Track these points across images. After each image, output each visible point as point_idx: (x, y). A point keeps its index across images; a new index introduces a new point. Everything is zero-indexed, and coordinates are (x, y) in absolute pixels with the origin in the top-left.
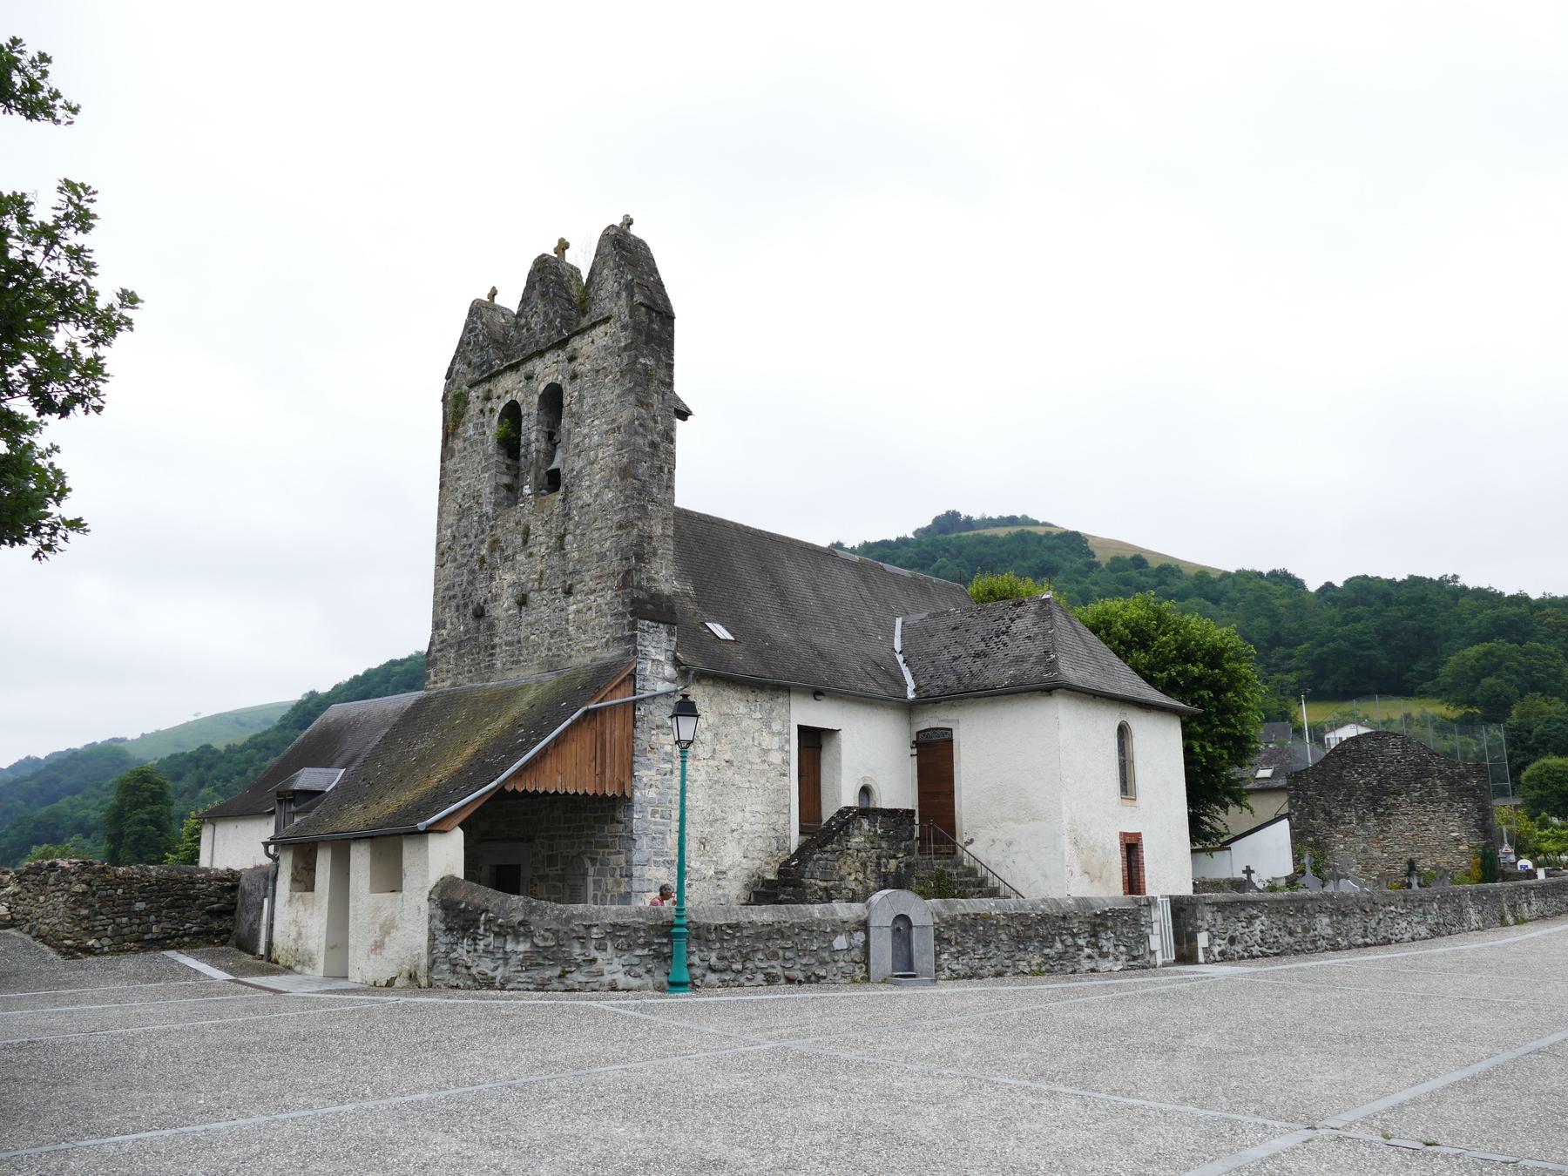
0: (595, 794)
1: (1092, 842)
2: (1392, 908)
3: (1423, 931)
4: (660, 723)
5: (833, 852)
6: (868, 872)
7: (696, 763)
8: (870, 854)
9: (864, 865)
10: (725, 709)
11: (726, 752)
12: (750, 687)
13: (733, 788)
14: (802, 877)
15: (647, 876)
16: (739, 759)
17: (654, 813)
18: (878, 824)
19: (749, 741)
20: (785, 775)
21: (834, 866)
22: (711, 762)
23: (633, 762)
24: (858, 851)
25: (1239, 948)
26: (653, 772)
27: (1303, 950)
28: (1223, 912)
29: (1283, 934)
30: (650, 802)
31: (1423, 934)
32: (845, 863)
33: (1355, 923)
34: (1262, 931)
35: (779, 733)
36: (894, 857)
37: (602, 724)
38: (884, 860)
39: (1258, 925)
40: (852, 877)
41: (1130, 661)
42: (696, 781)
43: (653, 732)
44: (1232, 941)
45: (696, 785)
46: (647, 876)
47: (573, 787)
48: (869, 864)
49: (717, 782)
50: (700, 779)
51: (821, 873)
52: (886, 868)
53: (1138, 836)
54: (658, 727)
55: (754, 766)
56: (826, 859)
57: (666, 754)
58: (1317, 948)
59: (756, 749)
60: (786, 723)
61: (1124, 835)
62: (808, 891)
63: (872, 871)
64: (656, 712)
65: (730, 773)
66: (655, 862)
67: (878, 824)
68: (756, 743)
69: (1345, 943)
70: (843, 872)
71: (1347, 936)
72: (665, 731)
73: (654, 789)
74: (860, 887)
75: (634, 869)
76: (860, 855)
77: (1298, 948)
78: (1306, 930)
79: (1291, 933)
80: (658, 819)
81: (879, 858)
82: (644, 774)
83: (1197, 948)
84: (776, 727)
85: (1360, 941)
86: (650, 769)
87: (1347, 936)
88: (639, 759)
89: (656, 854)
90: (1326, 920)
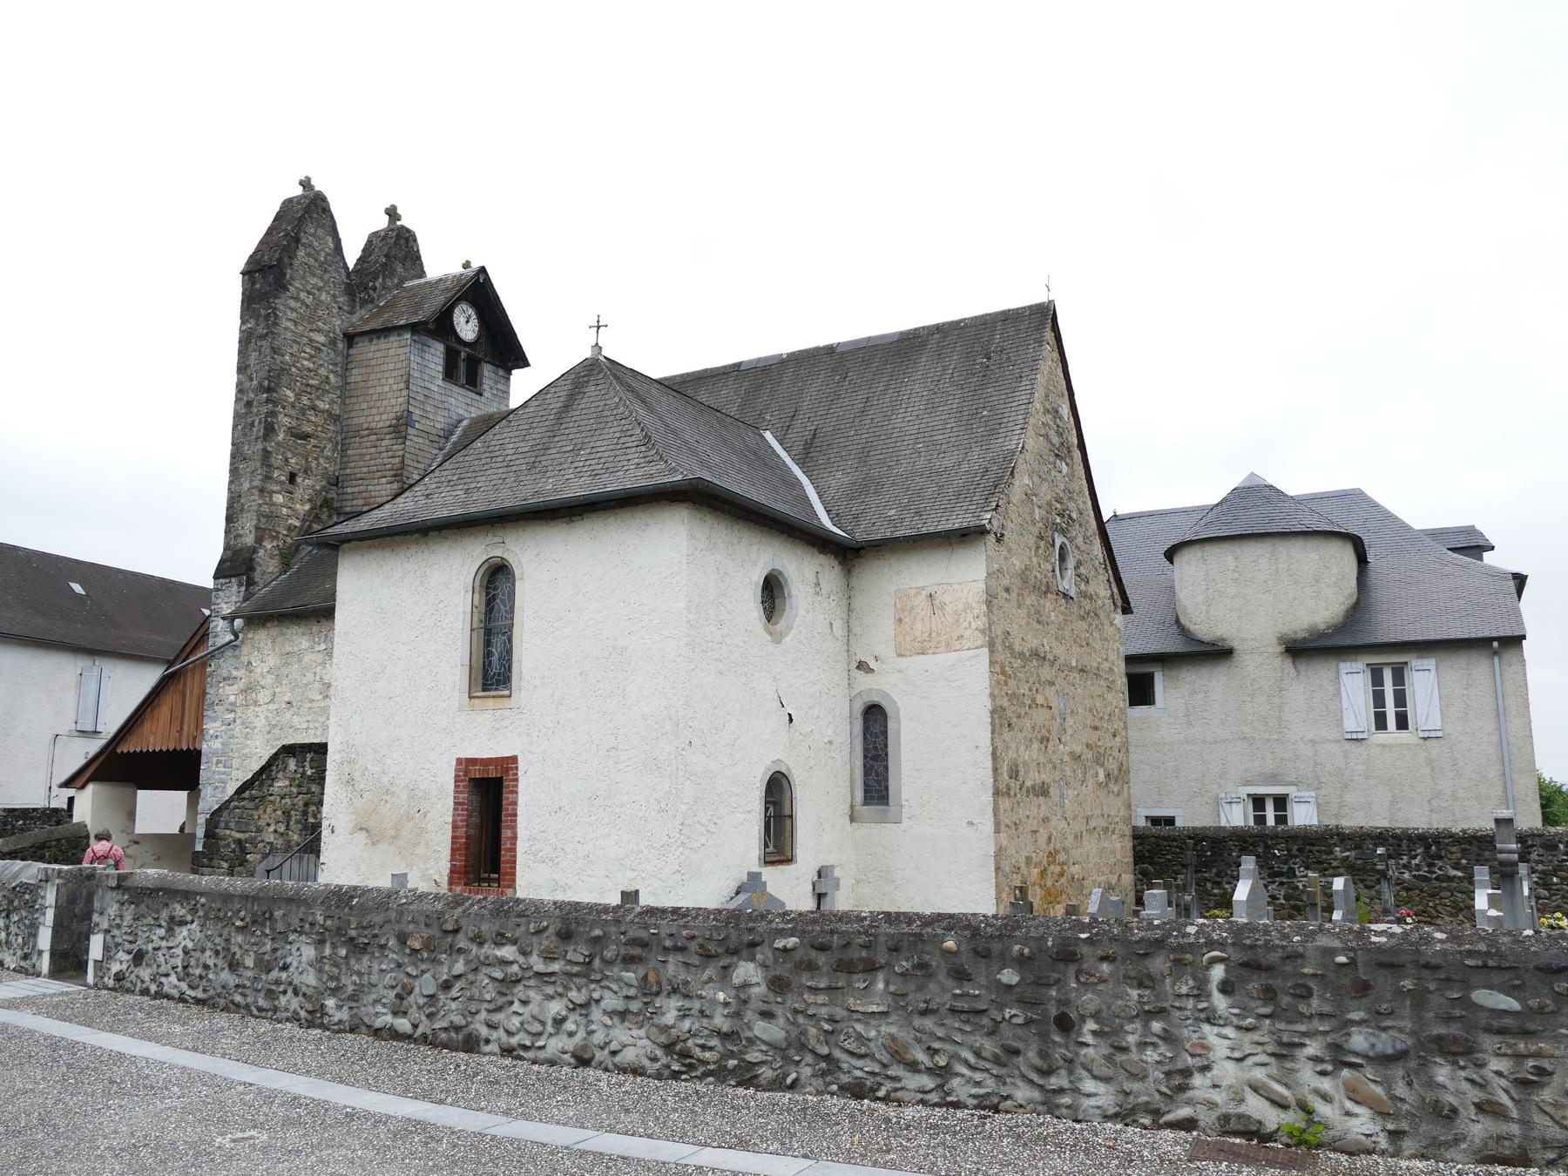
0: (175, 749)
1: (385, 780)
2: (508, 952)
3: (636, 1044)
5: (252, 799)
6: (292, 823)
7: (256, 709)
9: (287, 814)
10: (288, 648)
12: (314, 617)
13: (292, 730)
16: (299, 699)
17: (218, 762)
18: (307, 764)
19: (310, 676)
22: (271, 706)
23: (203, 716)
25: (145, 973)
26: (218, 724)
27: (247, 1007)
28: (137, 905)
29: (220, 963)
30: (215, 753)
31: (629, 1055)
33: (380, 971)
34: (186, 952)
37: (185, 685)
39: (185, 937)
40: (271, 829)
41: (233, 486)
42: (255, 727)
44: (138, 958)
45: (256, 731)
49: (275, 725)
51: (237, 822)
53: (508, 764)
54: (224, 679)
57: (231, 704)
58: (275, 1009)
59: (317, 685)
61: (465, 764)
62: (222, 843)
63: (297, 822)
64: (223, 665)
65: (288, 715)
67: (307, 764)
68: (318, 678)
69: (344, 1015)
70: (262, 823)
71: (354, 997)
72: (231, 682)
73: (220, 740)
74: (280, 841)
75: (451, 820)
76: (283, 801)
77: (238, 998)
78: (264, 966)
79: (234, 966)
81: (306, 805)
82: (211, 727)
83: (87, 962)
85: (387, 1019)
87: (354, 997)
90: (309, 952)
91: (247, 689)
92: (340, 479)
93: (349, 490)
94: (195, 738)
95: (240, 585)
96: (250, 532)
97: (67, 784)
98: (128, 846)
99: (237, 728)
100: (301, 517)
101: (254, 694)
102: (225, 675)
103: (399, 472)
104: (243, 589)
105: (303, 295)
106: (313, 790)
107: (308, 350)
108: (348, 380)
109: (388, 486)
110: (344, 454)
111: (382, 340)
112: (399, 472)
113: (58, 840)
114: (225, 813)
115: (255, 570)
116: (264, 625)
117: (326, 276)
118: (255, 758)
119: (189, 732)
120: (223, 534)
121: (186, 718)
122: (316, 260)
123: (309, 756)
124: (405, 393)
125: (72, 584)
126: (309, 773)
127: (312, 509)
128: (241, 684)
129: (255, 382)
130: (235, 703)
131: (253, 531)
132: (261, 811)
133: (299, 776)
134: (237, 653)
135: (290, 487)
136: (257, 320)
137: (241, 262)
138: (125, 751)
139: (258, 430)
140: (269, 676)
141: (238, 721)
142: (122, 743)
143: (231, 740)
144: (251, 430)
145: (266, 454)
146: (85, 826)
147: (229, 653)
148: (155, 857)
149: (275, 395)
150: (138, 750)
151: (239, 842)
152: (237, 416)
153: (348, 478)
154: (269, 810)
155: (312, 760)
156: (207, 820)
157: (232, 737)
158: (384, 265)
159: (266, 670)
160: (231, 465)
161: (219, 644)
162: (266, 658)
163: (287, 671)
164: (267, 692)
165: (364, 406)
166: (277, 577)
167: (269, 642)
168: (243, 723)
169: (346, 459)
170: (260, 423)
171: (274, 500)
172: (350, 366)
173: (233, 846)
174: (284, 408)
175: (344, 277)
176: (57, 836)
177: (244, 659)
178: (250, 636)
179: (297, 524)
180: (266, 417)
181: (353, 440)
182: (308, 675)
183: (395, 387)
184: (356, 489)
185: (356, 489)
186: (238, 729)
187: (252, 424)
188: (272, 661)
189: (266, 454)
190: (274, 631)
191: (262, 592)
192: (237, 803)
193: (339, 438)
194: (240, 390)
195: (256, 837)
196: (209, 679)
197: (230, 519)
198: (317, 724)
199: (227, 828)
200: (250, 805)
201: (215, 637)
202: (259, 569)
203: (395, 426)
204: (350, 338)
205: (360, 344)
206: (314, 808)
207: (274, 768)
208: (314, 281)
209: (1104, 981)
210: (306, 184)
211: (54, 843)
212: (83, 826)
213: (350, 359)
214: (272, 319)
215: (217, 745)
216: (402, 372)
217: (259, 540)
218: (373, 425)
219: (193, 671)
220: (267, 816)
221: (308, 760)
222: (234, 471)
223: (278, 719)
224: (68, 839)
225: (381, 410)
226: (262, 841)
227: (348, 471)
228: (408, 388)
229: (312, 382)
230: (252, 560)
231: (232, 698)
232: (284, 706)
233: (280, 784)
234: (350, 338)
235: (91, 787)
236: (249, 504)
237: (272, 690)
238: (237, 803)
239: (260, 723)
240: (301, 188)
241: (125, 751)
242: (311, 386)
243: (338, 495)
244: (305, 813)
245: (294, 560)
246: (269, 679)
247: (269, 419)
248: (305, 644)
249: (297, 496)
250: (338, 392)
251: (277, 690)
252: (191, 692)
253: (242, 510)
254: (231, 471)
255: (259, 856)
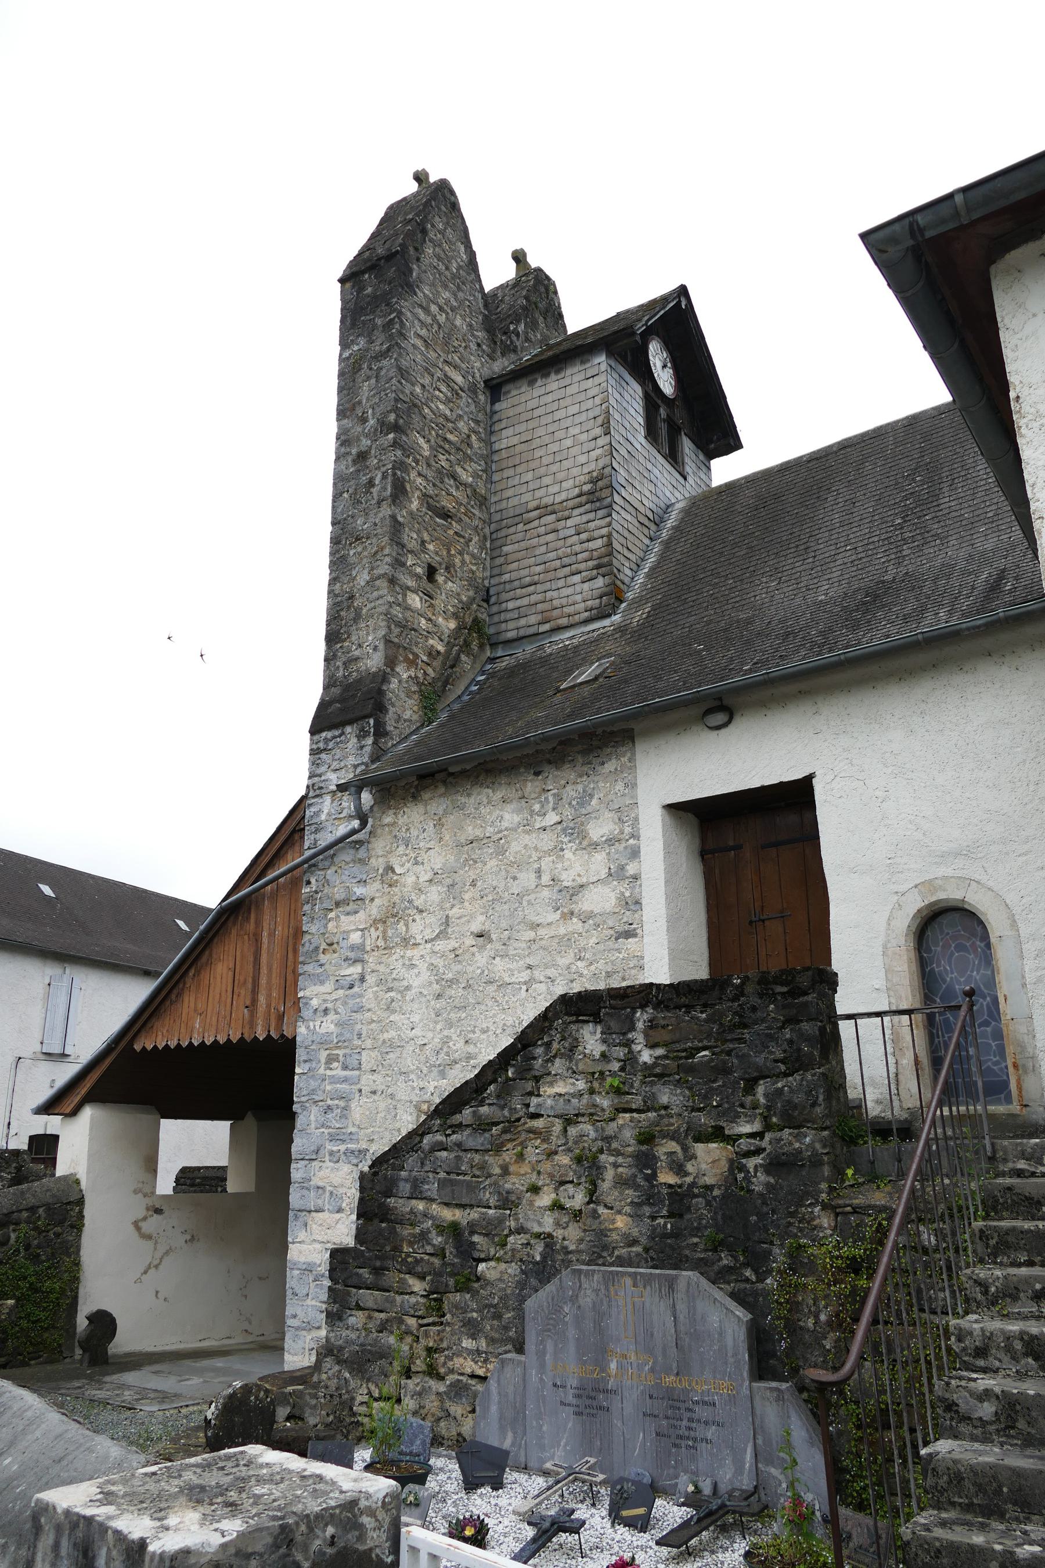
0: (242, 1039)
4: (343, 896)
5: (482, 1126)
6: (605, 1185)
7: (409, 953)
8: (611, 1128)
10: (471, 831)
11: (472, 916)
12: (529, 766)
13: (491, 988)
14: (389, 1194)
15: (316, 1181)
16: (504, 925)
17: (330, 1060)
18: (639, 1037)
19: (527, 879)
20: (629, 934)
21: (483, 1166)
22: (441, 945)
23: (296, 975)
24: (569, 1121)
26: (328, 987)
32: (521, 1157)
35: (611, 841)
36: (718, 1134)
37: (258, 923)
38: (667, 1147)
40: (545, 1199)
42: (408, 988)
43: (332, 915)
45: (409, 995)
46: (316, 1181)
47: (213, 1031)
48: (605, 1158)
49: (451, 982)
50: (415, 984)
51: (442, 1183)
52: (679, 1169)
54: (337, 904)
55: (542, 932)
56: (459, 1145)
57: (352, 948)
59: (546, 893)
60: (628, 814)
62: (406, 1231)
63: (621, 1183)
65: (481, 959)
66: (332, 1153)
67: (639, 1037)
68: (546, 879)
72: (352, 907)
73: (332, 1016)
76: (573, 1131)
80: (340, 1073)
81: (647, 1138)
84: (599, 829)
86: (322, 983)
88: (306, 968)
89: (332, 1138)
91: (391, 915)
92: (492, 591)
93: (511, 605)
94: (281, 1017)
95: (362, 735)
96: (375, 649)
97: (48, 1108)
98: (145, 1219)
99: (369, 994)
100: (445, 637)
101: (401, 927)
102: (339, 894)
103: (606, 560)
104: (370, 741)
105: (434, 308)
106: (664, 1099)
107: (444, 389)
108: (496, 447)
109: (586, 586)
110: (496, 553)
111: (553, 377)
112: (606, 560)
113: (32, 1209)
114: (411, 1161)
115: (387, 711)
116: (415, 797)
117: (460, 295)
118: (410, 1048)
119: (269, 1006)
120: (321, 664)
121: (263, 981)
122: (447, 268)
123: (641, 1018)
124: (603, 441)
125: (40, 885)
126: (646, 1056)
127: (459, 629)
128: (374, 910)
129: (372, 422)
130: (363, 945)
131: (381, 647)
132: (508, 1156)
133: (616, 1066)
134: (362, 853)
135: (429, 587)
136: (370, 335)
137: (339, 269)
138: (149, 1047)
139: (382, 488)
140: (434, 889)
141: (371, 979)
142: (143, 1034)
143: (358, 1016)
144: (368, 492)
145: (396, 527)
146: (78, 1182)
147: (346, 856)
148: (188, 1237)
149: (404, 438)
150: (173, 1044)
151: (454, 1230)
152: (340, 479)
153: (508, 587)
154: (532, 1153)
155: (652, 1025)
156: (362, 1177)
157: (360, 1009)
158: (525, 308)
159: (425, 877)
160: (332, 554)
161: (322, 844)
162: (424, 856)
163: (473, 874)
164: (431, 919)
165: (529, 476)
166: (417, 729)
167: (430, 826)
168: (380, 982)
169: (499, 561)
170: (384, 477)
171: (410, 602)
172: (496, 427)
173: (438, 1240)
174: (417, 462)
175: (481, 305)
176: (32, 1201)
177: (378, 864)
178: (388, 819)
179: (441, 648)
180: (393, 468)
181: (512, 530)
182: (521, 876)
183: (584, 437)
184: (525, 601)
185: (525, 601)
186: (370, 994)
187: (371, 483)
188: (437, 859)
189: (396, 527)
190: (437, 804)
191: (398, 746)
192: (439, 1137)
193: (487, 531)
194: (344, 440)
195: (501, 1221)
196: (307, 908)
197: (333, 637)
198: (551, 972)
199: (416, 1194)
200: (480, 1141)
201: (317, 831)
202: (391, 710)
203: (590, 493)
204: (495, 388)
205: (514, 393)
206: (673, 1146)
207: (539, 1051)
208: (446, 295)
209: (521, 1260)
210: (420, 177)
211: (25, 1214)
212: (73, 1181)
213: (496, 418)
214: (397, 326)
215: (327, 1026)
216: (597, 411)
217: (391, 662)
218: (548, 500)
219: (274, 896)
220: (525, 1168)
221: (640, 1025)
222: (339, 564)
223: (458, 967)
224: (48, 1207)
225: (561, 476)
226: (520, 1230)
227: (506, 577)
228: (607, 433)
229: (450, 437)
230: (381, 693)
231: (355, 938)
232: (470, 941)
233: (560, 1088)
234: (495, 388)
235: (88, 1113)
236: (369, 606)
237: (440, 915)
238: (439, 1137)
239: (419, 979)
240: (416, 185)
241: (149, 1047)
242: (449, 442)
243: (490, 616)
244: (645, 1161)
245: (440, 706)
246: (434, 894)
247: (399, 473)
248: (510, 817)
249: (439, 602)
250: (482, 463)
251: (451, 913)
252: (271, 935)
253: (357, 618)
254: (333, 564)
255: (513, 1269)
